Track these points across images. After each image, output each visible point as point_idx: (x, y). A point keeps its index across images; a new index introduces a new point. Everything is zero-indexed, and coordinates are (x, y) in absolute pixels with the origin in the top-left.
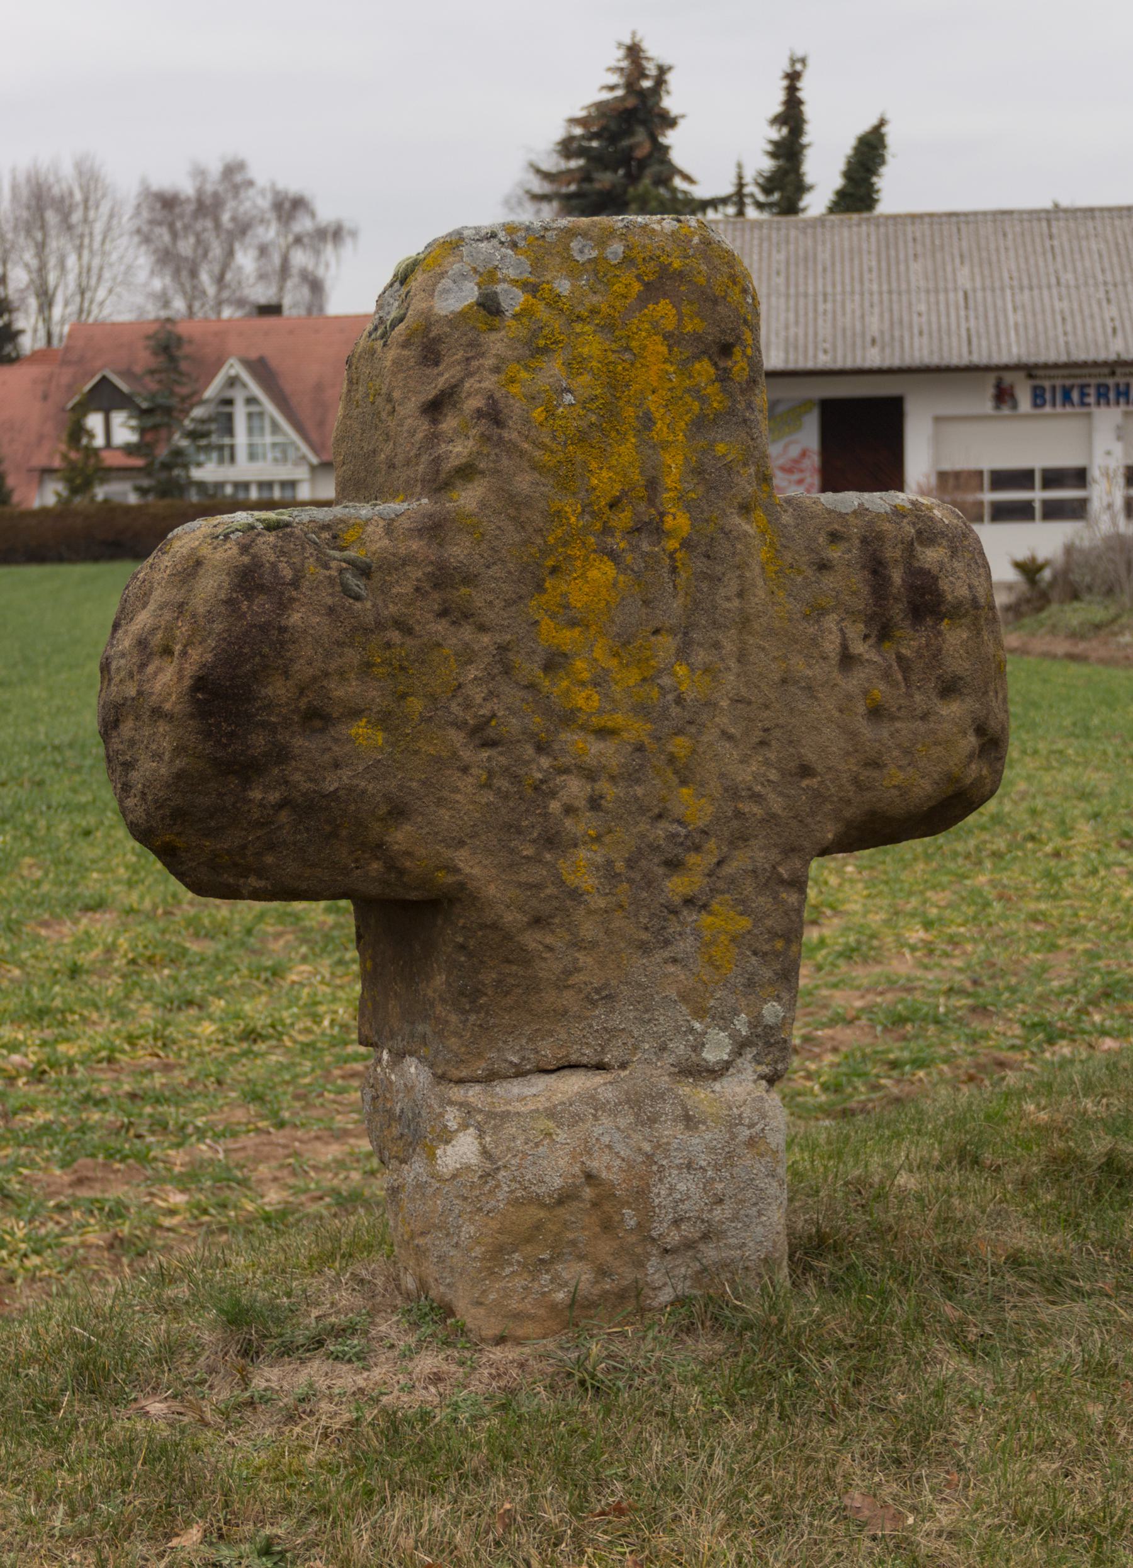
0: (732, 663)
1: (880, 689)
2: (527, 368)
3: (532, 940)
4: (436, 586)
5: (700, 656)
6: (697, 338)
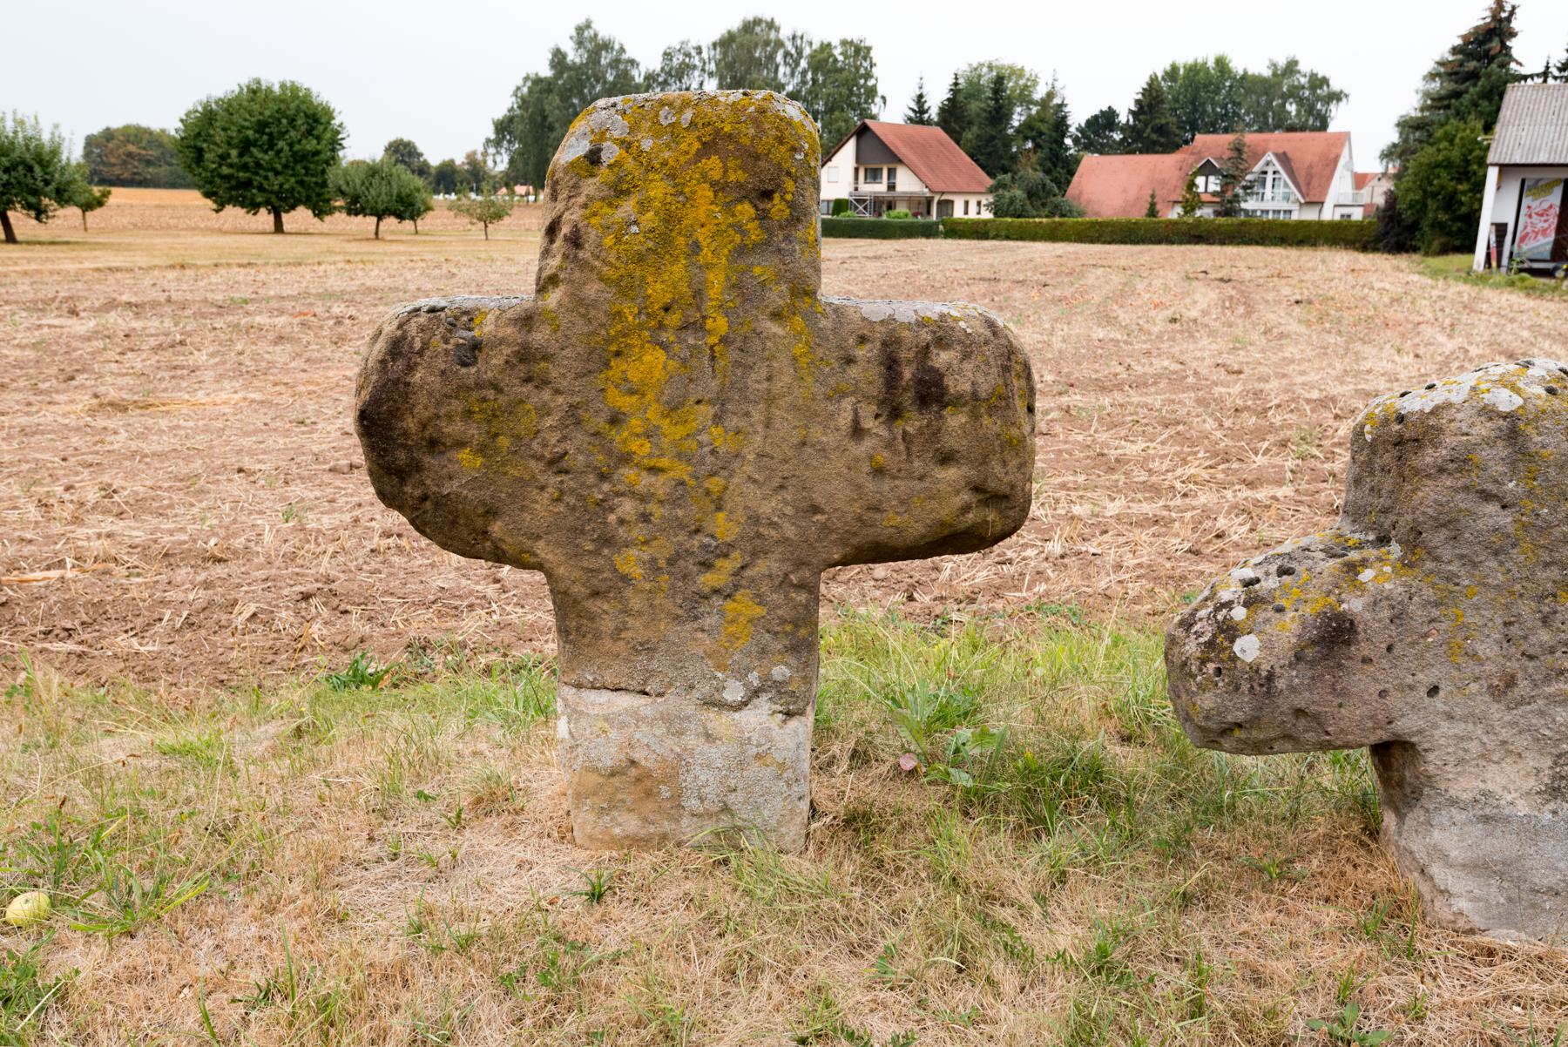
0: (760, 428)
1: (883, 457)
2: (610, 205)
3: (594, 606)
4: (521, 361)
5: (734, 422)
6: (740, 185)
